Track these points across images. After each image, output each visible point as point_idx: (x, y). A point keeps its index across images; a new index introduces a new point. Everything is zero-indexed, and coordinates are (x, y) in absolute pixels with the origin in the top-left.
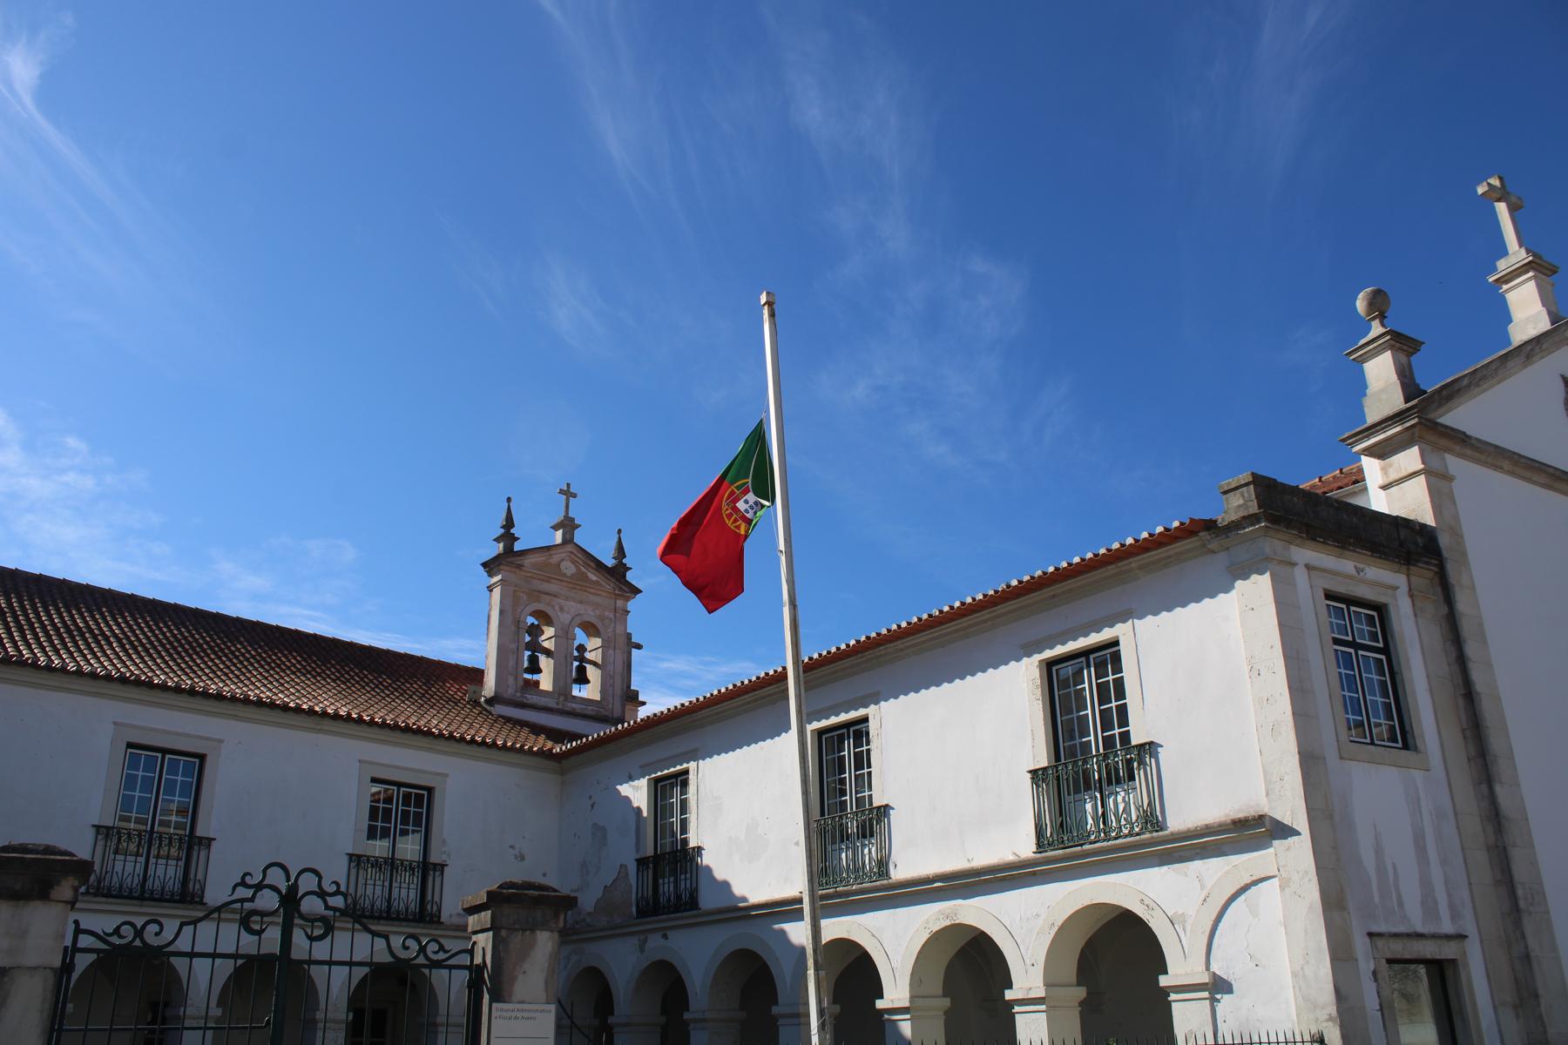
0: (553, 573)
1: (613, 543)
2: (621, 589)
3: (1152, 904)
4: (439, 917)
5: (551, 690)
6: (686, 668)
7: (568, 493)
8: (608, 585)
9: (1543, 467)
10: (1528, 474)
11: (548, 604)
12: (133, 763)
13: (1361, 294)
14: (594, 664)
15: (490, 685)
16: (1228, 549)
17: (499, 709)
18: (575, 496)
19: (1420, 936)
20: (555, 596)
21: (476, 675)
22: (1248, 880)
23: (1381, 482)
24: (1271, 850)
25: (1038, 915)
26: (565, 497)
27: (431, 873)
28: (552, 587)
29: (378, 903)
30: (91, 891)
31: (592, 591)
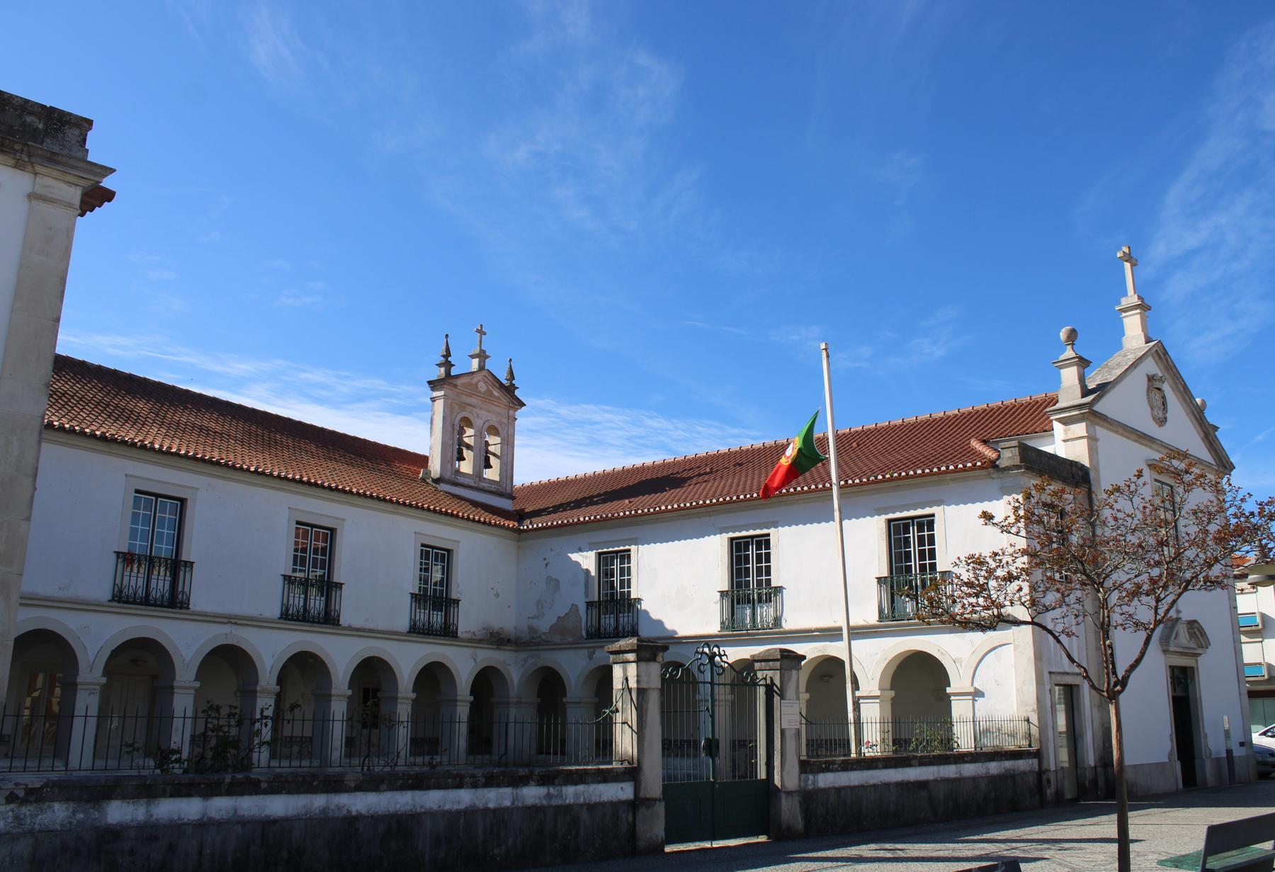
0: (472, 390)
1: (507, 369)
2: (513, 403)
3: (944, 652)
4: (457, 633)
5: (471, 473)
6: (324, 380)
7: (481, 332)
8: (505, 400)
11: (470, 412)
12: (137, 502)
13: (1064, 330)
14: (495, 455)
15: (435, 467)
16: (1001, 478)
17: (443, 487)
18: (485, 334)
19: (1068, 674)
20: (474, 407)
21: (422, 461)
22: (1005, 643)
23: (1063, 438)
24: (1010, 631)
25: (877, 654)
26: (479, 334)
27: (183, 568)
28: (472, 400)
29: (140, 591)
30: (116, 599)
31: (496, 403)
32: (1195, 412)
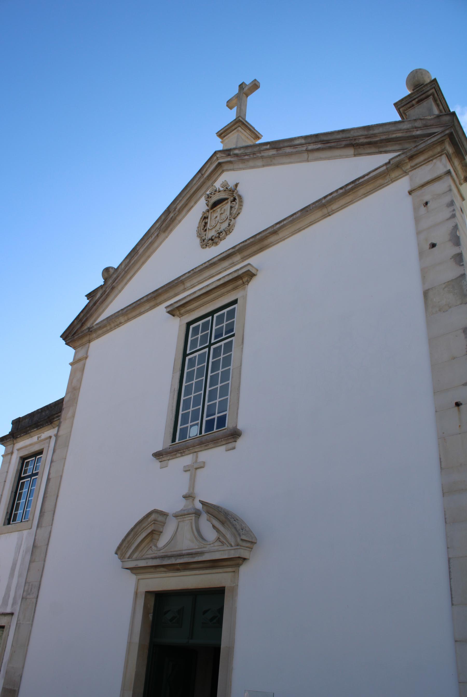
9: (138, 303)
10: (137, 312)
32: (310, 147)
